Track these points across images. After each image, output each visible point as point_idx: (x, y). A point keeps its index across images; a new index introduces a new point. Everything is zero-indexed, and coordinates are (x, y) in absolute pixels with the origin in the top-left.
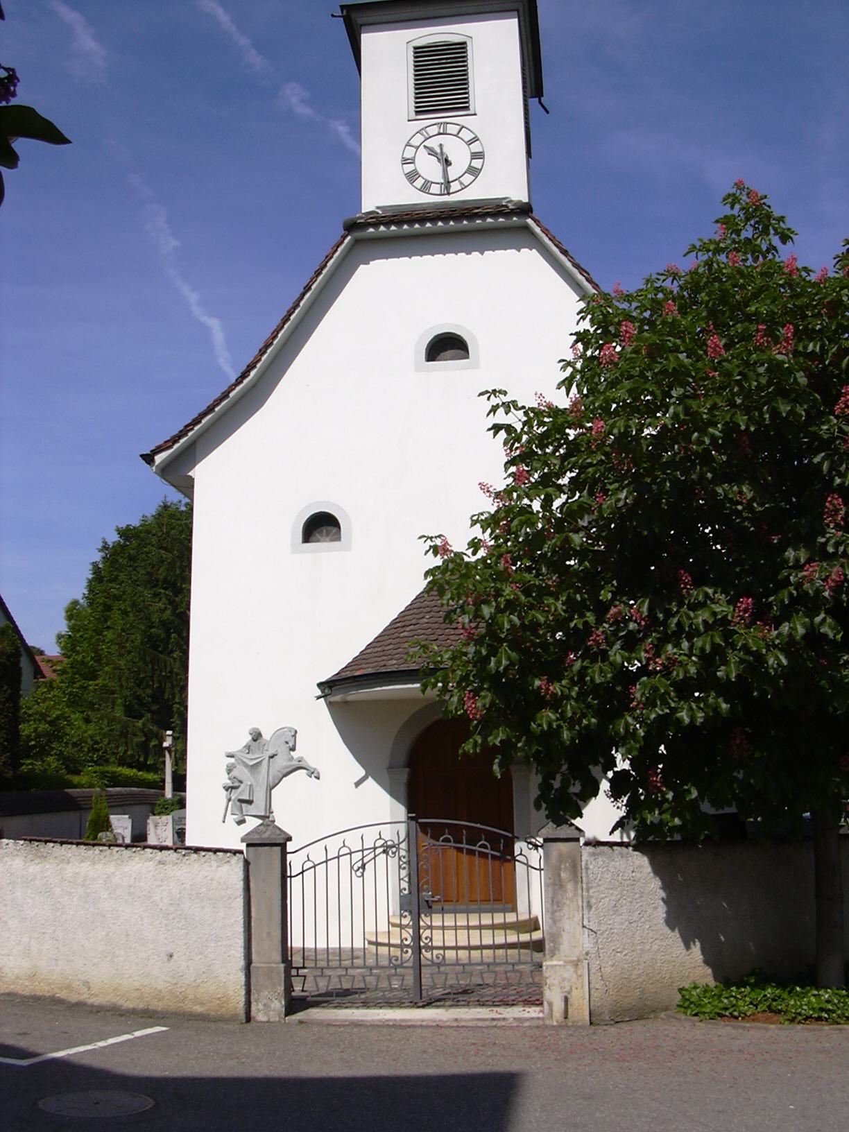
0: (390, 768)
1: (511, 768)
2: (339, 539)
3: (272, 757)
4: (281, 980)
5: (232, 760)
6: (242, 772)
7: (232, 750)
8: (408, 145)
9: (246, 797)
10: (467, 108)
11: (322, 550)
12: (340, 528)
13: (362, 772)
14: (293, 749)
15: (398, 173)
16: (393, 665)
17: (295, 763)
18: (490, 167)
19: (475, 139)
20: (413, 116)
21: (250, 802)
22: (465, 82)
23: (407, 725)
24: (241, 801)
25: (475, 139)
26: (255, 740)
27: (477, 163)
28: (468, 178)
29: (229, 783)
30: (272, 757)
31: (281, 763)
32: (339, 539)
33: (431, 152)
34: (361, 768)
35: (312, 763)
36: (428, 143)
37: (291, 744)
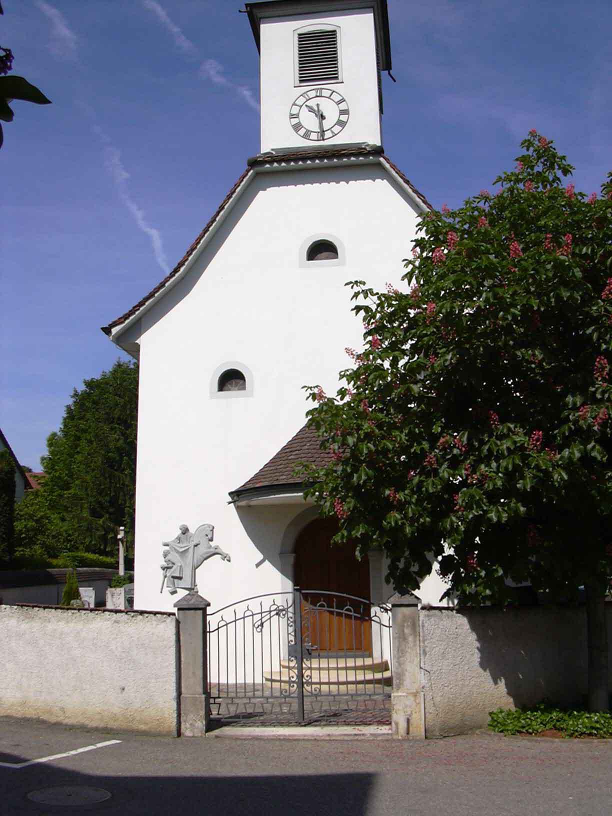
2: (244, 389)
3: (196, 546)
5: (167, 548)
6: (174, 557)
7: (167, 541)
8: (294, 104)
9: (177, 575)
10: (337, 78)
11: (232, 397)
12: (245, 380)
14: (211, 540)
15: (287, 125)
17: (213, 550)
19: (343, 100)
21: (180, 578)
22: (335, 59)
24: (174, 577)
25: (343, 100)
27: (344, 118)
28: (337, 129)
29: (165, 565)
30: (196, 546)
31: (202, 550)
32: (244, 389)
33: (311, 109)
35: (224, 549)
37: (210, 536)
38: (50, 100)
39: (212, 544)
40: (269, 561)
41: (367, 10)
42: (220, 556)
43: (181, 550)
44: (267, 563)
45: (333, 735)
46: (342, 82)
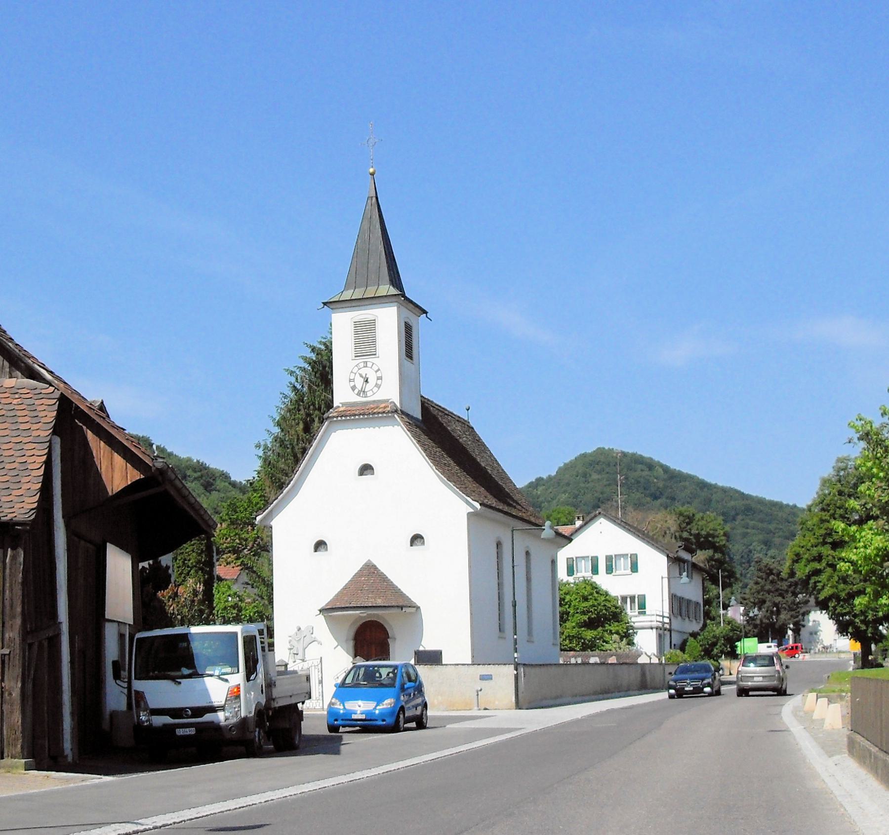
0: (347, 640)
1: (273, 706)
2: (373, 474)
3: (305, 637)
4: (72, 779)
5: (290, 638)
6: (294, 643)
7: (290, 635)
8: (352, 372)
9: (295, 652)
10: (375, 354)
11: (366, 478)
12: (373, 469)
13: (337, 644)
14: (312, 634)
15: (348, 386)
16: (338, 605)
17: (313, 640)
18: (384, 383)
19: (379, 370)
20: (354, 358)
21: (297, 654)
22: (374, 341)
23: (354, 623)
24: (294, 654)
25: (379, 370)
26: (298, 630)
27: (379, 382)
28: (375, 389)
29: (290, 647)
30: (305, 637)
31: (307, 640)
32: (373, 474)
33: (361, 376)
34: (335, 641)
35: (319, 639)
36: (360, 372)
37: (311, 632)
38: (404, 324)
39: (313, 636)
40: (342, 647)
41: (391, 304)
42: (316, 642)
43: (297, 639)
44: (339, 647)
45: (446, 410)
46: (378, 357)
